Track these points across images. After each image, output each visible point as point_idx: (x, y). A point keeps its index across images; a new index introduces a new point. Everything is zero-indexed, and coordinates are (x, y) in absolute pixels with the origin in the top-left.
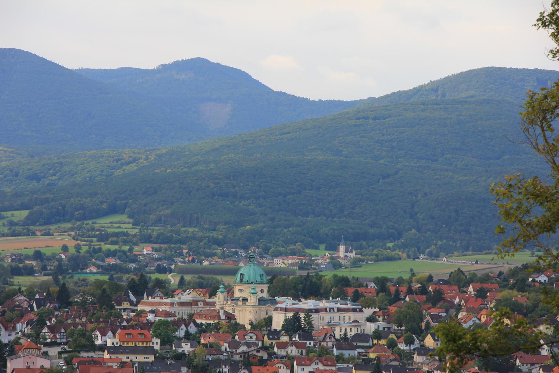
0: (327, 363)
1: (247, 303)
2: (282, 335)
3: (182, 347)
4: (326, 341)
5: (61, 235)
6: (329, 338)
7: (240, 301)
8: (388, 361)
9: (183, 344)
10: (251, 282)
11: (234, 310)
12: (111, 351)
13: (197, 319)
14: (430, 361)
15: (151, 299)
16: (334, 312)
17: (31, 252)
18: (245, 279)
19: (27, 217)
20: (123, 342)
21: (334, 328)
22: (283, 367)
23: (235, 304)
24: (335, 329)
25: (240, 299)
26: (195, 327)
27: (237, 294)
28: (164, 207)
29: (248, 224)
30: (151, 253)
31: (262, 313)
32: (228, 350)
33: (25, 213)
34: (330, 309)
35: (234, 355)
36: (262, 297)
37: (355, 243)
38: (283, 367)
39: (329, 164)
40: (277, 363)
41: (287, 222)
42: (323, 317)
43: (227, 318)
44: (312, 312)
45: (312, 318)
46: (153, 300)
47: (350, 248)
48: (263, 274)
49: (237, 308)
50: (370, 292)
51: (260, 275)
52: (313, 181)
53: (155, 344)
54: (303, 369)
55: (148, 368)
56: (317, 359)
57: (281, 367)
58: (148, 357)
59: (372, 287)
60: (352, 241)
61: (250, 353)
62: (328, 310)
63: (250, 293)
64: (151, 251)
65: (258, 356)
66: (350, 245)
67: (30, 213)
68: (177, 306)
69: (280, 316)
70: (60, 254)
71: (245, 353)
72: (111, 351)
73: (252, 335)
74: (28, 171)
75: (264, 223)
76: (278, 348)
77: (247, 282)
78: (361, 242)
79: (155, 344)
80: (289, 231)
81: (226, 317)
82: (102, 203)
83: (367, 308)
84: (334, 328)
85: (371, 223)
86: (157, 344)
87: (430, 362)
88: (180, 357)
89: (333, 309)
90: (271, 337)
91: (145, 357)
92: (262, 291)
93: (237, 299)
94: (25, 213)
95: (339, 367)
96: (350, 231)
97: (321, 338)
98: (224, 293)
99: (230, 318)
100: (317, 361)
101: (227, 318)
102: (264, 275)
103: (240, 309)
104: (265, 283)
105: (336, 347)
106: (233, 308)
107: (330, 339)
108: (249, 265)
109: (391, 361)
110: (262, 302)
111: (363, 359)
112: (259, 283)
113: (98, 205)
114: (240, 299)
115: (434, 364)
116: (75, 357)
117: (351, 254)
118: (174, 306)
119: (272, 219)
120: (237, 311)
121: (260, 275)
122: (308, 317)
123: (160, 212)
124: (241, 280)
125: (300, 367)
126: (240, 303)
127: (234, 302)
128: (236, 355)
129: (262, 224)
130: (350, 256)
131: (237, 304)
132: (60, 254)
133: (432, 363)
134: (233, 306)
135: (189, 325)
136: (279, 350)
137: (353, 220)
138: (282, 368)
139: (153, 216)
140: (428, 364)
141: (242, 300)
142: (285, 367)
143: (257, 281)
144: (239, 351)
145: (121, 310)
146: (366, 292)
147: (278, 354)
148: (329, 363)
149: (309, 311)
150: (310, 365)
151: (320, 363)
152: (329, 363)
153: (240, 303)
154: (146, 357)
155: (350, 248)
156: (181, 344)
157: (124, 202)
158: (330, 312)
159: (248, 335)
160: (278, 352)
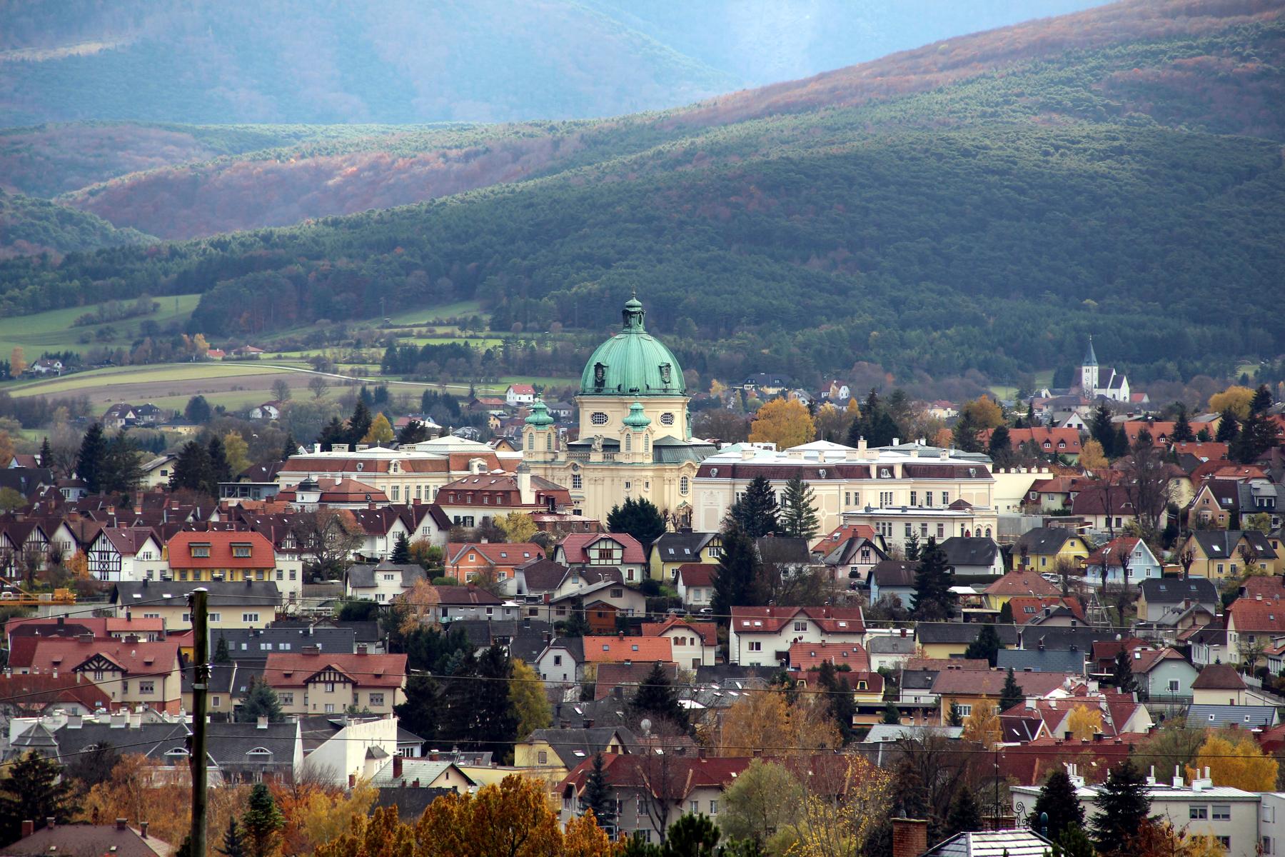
0: (836, 623)
1: (618, 458)
2: (707, 545)
3: (375, 586)
4: (851, 562)
5: (279, 357)
6: (859, 555)
7: (595, 450)
8: (1041, 616)
9: (379, 576)
10: (631, 391)
11: (577, 481)
12: (136, 596)
13: (448, 503)
14: (1184, 613)
15: (322, 451)
16: (893, 476)
17: (180, 404)
18: (612, 381)
19: (196, 314)
20: (183, 572)
21: (887, 527)
22: (692, 640)
23: (580, 458)
24: (890, 529)
25: (597, 445)
26: (440, 529)
27: (588, 430)
28: (584, 274)
29: (824, 318)
30: (532, 400)
31: (666, 487)
32: (526, 593)
33: (188, 303)
34: (879, 469)
35: (539, 607)
36: (669, 437)
37: (1141, 367)
38: (692, 640)
39: (1073, 142)
40: (672, 628)
41: (942, 311)
42: (856, 494)
43: (542, 499)
44: (819, 477)
45: (808, 495)
46: (325, 455)
47: (1114, 373)
48: (668, 365)
49: (586, 473)
50: (1063, 441)
51: (660, 367)
52: (1022, 192)
53: (286, 575)
54: (758, 647)
55: (244, 646)
56: (802, 611)
57: (684, 639)
58: (256, 616)
59: (1075, 426)
60: (1134, 361)
61: (586, 602)
62: (874, 472)
63: (626, 424)
64: (531, 396)
65: (614, 608)
66: (1127, 372)
67: (203, 301)
68: (400, 471)
69: (715, 492)
70: (267, 408)
71: (575, 600)
72: (136, 596)
73: (609, 546)
74: (599, 366)
75: (873, 313)
76: (688, 585)
77: (616, 391)
78: (1161, 362)
79: (286, 575)
80: (944, 335)
81: (538, 497)
82: (408, 268)
83: (1002, 470)
84: (887, 527)
85: (1195, 308)
86: (293, 575)
87: (1182, 620)
88: (361, 614)
89: (891, 469)
90: (672, 551)
91: (245, 617)
92: (667, 419)
93: (587, 447)
94: (188, 303)
95: (874, 635)
96: (1129, 332)
97: (835, 557)
98: (547, 427)
99: (553, 500)
100: (801, 619)
101: (542, 499)
102: (673, 368)
103: (598, 474)
104: (674, 392)
105: (876, 579)
106: (575, 473)
107: (863, 555)
108: (623, 336)
109: (1049, 615)
110: (666, 454)
111: (966, 614)
112: (657, 392)
113: (398, 275)
114: (597, 445)
115: (1194, 624)
116: (12, 617)
117: (1115, 391)
118: (391, 471)
119: (896, 304)
120: (585, 483)
121: (660, 367)
122: (796, 494)
123: (569, 288)
124: (600, 384)
125: (746, 641)
126: (596, 457)
127: (577, 454)
128: (546, 607)
129: (867, 318)
130: (1114, 396)
131: (586, 460)
132: (267, 408)
133: (1190, 622)
134: (575, 467)
135: (418, 523)
136: (692, 593)
137: (1141, 303)
138: (688, 641)
139: (550, 299)
140: (1176, 626)
141: (604, 446)
142: (697, 641)
143: (652, 386)
144: (559, 595)
145: (233, 490)
146: (1048, 441)
147: (689, 603)
148: (842, 624)
149: (796, 476)
150: (778, 632)
151: (810, 626)
152: (842, 624)
153: (596, 457)
154: (251, 616)
155: (1114, 373)
156: (373, 577)
157: (473, 265)
158: (879, 476)
159: (596, 546)
160: (687, 598)
